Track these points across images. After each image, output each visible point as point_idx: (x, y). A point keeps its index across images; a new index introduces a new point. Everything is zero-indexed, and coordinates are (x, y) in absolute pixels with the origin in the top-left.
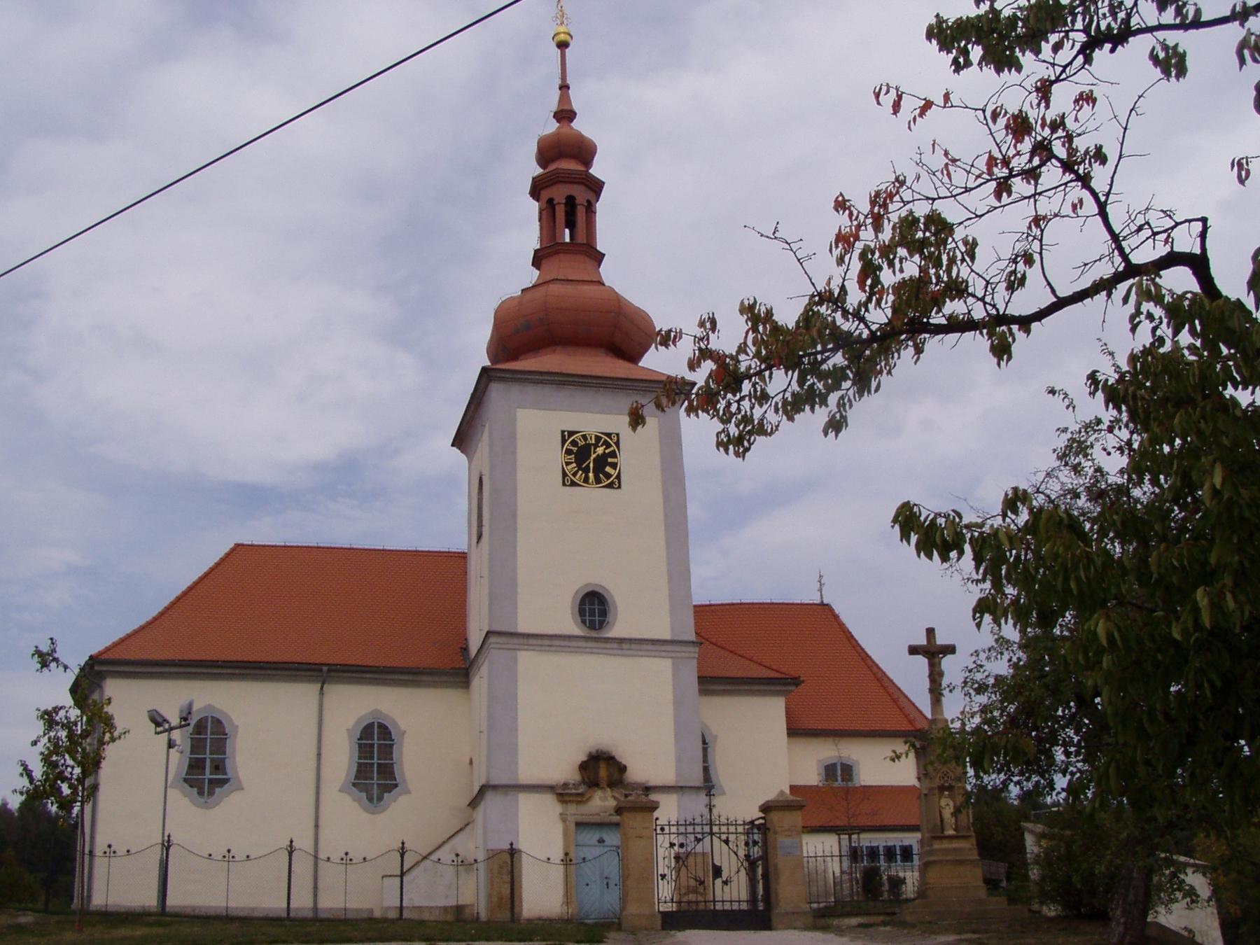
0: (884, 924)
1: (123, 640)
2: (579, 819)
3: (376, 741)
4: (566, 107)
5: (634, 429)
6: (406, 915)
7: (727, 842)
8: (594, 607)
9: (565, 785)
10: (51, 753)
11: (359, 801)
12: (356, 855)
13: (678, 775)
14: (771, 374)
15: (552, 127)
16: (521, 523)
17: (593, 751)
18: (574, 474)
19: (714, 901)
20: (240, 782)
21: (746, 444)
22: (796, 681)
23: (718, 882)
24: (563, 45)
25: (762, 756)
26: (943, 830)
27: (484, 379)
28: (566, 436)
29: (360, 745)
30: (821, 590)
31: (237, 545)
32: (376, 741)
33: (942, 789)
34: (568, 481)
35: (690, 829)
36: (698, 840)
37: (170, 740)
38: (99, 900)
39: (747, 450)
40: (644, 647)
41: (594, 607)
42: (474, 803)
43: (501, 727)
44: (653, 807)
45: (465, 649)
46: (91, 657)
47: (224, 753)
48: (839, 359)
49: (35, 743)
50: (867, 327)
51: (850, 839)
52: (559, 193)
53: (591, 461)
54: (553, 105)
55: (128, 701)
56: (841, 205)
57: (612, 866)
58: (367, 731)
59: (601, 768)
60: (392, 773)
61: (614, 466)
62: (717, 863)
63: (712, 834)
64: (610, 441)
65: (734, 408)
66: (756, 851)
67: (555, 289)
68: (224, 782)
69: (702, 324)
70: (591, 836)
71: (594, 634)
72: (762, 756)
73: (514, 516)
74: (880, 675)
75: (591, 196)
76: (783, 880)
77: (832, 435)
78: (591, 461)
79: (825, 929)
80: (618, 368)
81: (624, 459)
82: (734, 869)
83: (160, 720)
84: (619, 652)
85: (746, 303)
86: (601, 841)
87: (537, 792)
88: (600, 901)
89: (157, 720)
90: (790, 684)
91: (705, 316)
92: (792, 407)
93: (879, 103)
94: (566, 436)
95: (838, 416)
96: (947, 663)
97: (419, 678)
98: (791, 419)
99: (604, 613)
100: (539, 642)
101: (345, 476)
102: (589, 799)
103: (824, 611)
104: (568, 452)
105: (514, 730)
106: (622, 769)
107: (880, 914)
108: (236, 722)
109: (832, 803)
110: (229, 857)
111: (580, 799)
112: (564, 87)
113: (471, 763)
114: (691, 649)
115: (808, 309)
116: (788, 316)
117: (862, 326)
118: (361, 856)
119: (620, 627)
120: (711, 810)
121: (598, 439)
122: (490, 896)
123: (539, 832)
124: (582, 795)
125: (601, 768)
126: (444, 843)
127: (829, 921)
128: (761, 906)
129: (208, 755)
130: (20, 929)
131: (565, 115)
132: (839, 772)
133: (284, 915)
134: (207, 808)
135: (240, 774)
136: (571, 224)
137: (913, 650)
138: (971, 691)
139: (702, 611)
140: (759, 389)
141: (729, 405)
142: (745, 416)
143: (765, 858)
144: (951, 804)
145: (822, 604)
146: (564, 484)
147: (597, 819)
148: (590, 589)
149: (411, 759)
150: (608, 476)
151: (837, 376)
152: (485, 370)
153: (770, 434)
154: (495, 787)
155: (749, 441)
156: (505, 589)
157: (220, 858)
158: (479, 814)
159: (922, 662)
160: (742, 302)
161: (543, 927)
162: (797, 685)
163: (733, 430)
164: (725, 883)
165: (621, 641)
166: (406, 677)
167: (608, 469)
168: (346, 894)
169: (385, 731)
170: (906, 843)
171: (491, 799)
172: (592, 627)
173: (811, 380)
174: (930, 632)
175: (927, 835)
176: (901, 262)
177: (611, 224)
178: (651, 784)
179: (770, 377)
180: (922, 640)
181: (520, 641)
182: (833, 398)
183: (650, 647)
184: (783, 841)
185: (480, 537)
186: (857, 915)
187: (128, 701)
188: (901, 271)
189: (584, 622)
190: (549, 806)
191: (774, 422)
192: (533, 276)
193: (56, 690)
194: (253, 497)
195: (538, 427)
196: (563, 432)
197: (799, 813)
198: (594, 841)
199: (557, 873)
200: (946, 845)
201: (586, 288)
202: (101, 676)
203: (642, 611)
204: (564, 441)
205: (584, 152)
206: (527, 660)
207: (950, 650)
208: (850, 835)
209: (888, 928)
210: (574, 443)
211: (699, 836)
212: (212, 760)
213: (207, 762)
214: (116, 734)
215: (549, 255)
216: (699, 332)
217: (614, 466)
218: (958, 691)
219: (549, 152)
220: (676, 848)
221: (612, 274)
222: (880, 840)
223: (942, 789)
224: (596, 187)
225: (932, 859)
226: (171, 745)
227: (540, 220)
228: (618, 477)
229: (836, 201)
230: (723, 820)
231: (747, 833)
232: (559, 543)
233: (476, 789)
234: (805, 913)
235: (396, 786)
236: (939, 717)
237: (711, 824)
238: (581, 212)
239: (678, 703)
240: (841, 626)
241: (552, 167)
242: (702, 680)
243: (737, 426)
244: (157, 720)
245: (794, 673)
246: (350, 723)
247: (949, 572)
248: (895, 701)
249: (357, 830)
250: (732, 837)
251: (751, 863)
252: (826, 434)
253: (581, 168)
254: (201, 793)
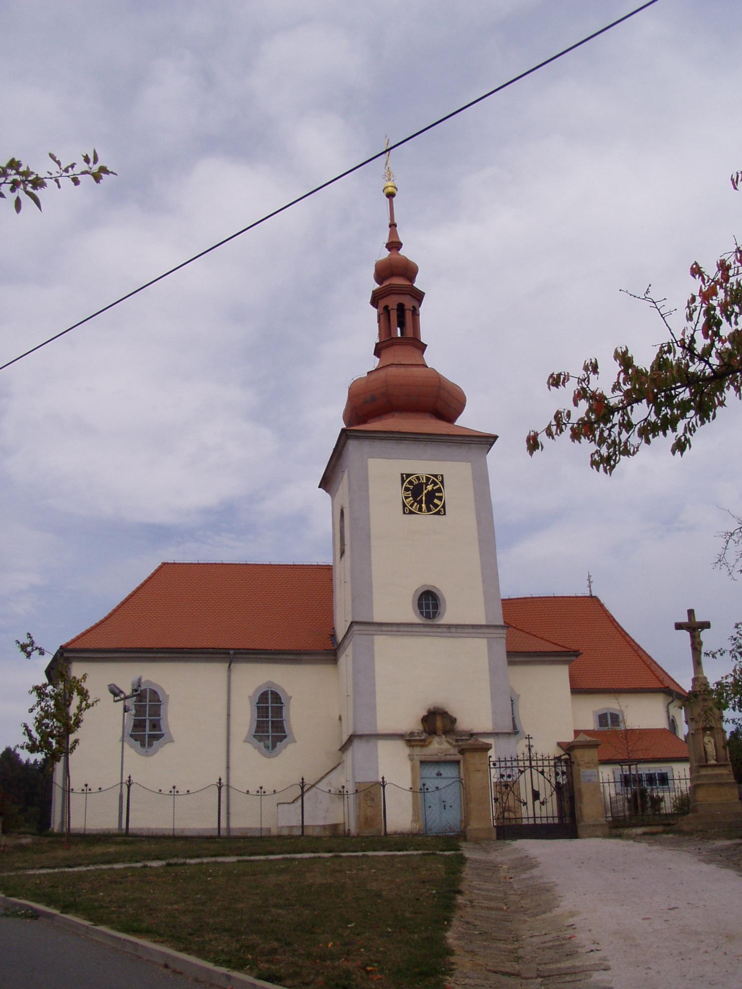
0: (667, 832)
1: (83, 634)
2: (423, 758)
3: (270, 704)
4: (395, 240)
5: (531, 454)
6: (307, 832)
7: (542, 773)
8: (429, 602)
9: (412, 734)
10: (43, 718)
11: (259, 749)
12: (269, 789)
13: (494, 724)
14: (632, 408)
15: (385, 254)
16: (374, 542)
17: (431, 707)
18: (412, 506)
19: (535, 817)
20: (171, 737)
21: (612, 463)
22: (576, 653)
23: (537, 803)
24: (391, 196)
25: (553, 710)
26: (707, 760)
27: (343, 437)
28: (404, 477)
29: (258, 707)
30: (590, 587)
31: (164, 564)
32: (270, 704)
33: (705, 729)
34: (407, 511)
35: (515, 764)
36: (521, 772)
37: (125, 706)
38: (77, 823)
39: (614, 466)
40: (467, 630)
41: (429, 602)
42: (344, 748)
43: (363, 691)
44: (486, 748)
45: (333, 636)
46: (61, 647)
47: (159, 715)
48: (685, 394)
49: (31, 710)
50: (711, 367)
51: (630, 768)
52: (392, 302)
53: (423, 496)
54: (385, 238)
55: (96, 677)
56: (696, 271)
57: (452, 794)
58: (263, 697)
59: (437, 721)
60: (282, 727)
61: (440, 498)
62: (536, 788)
63: (531, 767)
64: (437, 480)
65: (606, 434)
66: (562, 780)
67: (393, 371)
68: (157, 737)
69: (586, 368)
70: (431, 771)
71: (430, 622)
72: (553, 710)
73: (369, 536)
74: (636, 648)
75: (416, 304)
76: (586, 800)
77: (678, 453)
78: (423, 496)
79: (619, 836)
80: (440, 427)
81: (447, 494)
82: (548, 793)
83: (117, 692)
84: (449, 635)
85: (619, 351)
86: (439, 774)
87: (391, 739)
88: (445, 818)
89: (115, 692)
90: (572, 655)
91: (588, 361)
92: (648, 431)
93: (735, 188)
94: (404, 477)
95: (683, 438)
96: (704, 635)
97: (301, 657)
98: (648, 441)
99: (436, 606)
100: (390, 629)
101: (224, 517)
102: (430, 743)
103: (593, 601)
104: (407, 489)
105: (373, 694)
106: (453, 721)
107: (658, 825)
108: (167, 693)
109: (610, 740)
110: (261, 792)
111: (423, 744)
112: (393, 225)
113: (340, 719)
114: (501, 631)
115: (659, 357)
116: (644, 361)
117: (707, 366)
118: (264, 792)
119: (448, 616)
120: (530, 750)
121: (428, 479)
122: (358, 818)
123: (394, 767)
124: (424, 740)
125: (437, 721)
126: (322, 778)
127: (621, 831)
128: (567, 820)
129: (147, 717)
130: (22, 848)
131: (394, 245)
132: (608, 719)
133: (216, 833)
134: (148, 756)
135: (172, 730)
136: (401, 324)
137: (679, 626)
138: (737, 654)
139: (509, 605)
140: (626, 418)
141: (602, 432)
142: (614, 441)
143: (571, 784)
144: (712, 741)
145: (591, 597)
146: (404, 513)
147: (435, 758)
148: (426, 589)
149: (296, 717)
150: (436, 506)
151: (684, 407)
152: (343, 431)
153: (634, 453)
154: (361, 736)
155: (615, 461)
156: (363, 590)
157: (168, 793)
158: (348, 756)
159: (685, 635)
160: (616, 351)
161: (403, 841)
162: (577, 656)
163: (604, 451)
164: (542, 803)
165: (449, 626)
166: (291, 657)
167: (436, 501)
168: (246, 818)
169: (276, 697)
170: (664, 771)
171: (357, 744)
172: (428, 616)
173: (665, 411)
174: (691, 613)
175: (696, 764)
176: (736, 317)
177: (431, 321)
178: (475, 731)
179: (632, 410)
180: (685, 619)
181: (376, 628)
182: (681, 425)
183: (471, 630)
184: (585, 773)
185: (342, 553)
186: (641, 826)
187: (96, 677)
188: (736, 323)
189: (422, 613)
190: (400, 749)
191: (636, 444)
192: (375, 362)
193: (36, 671)
194: (160, 533)
195: (384, 471)
196: (402, 475)
197: (596, 750)
198: (434, 774)
199: (407, 798)
200: (710, 772)
201: (414, 369)
202: (69, 661)
203: (464, 605)
204: (403, 482)
205: (409, 271)
206: (382, 643)
207: (707, 625)
208: (630, 766)
209: (671, 836)
210: (410, 483)
211: (522, 769)
212: (151, 721)
213: (146, 722)
214: (90, 701)
215: (387, 347)
216: (582, 374)
217: (440, 498)
218: (727, 654)
219: (383, 272)
220: (505, 778)
221: (433, 359)
222: (644, 769)
223: (705, 729)
224: (419, 296)
225: (698, 782)
226: (126, 710)
227: (379, 322)
228: (444, 507)
229: (692, 268)
230: (539, 757)
231: (555, 766)
232: (403, 556)
233: (345, 738)
234: (602, 825)
235: (285, 737)
236: (700, 676)
237: (530, 760)
238: (408, 315)
239: (493, 670)
240: (606, 612)
241: (386, 283)
242: (509, 654)
243: (608, 449)
244: (115, 692)
245: (576, 648)
246: (251, 692)
247: (718, 565)
248: (648, 667)
249: (254, 769)
250: (546, 769)
251: (558, 788)
252: (674, 453)
253: (408, 283)
254: (143, 745)
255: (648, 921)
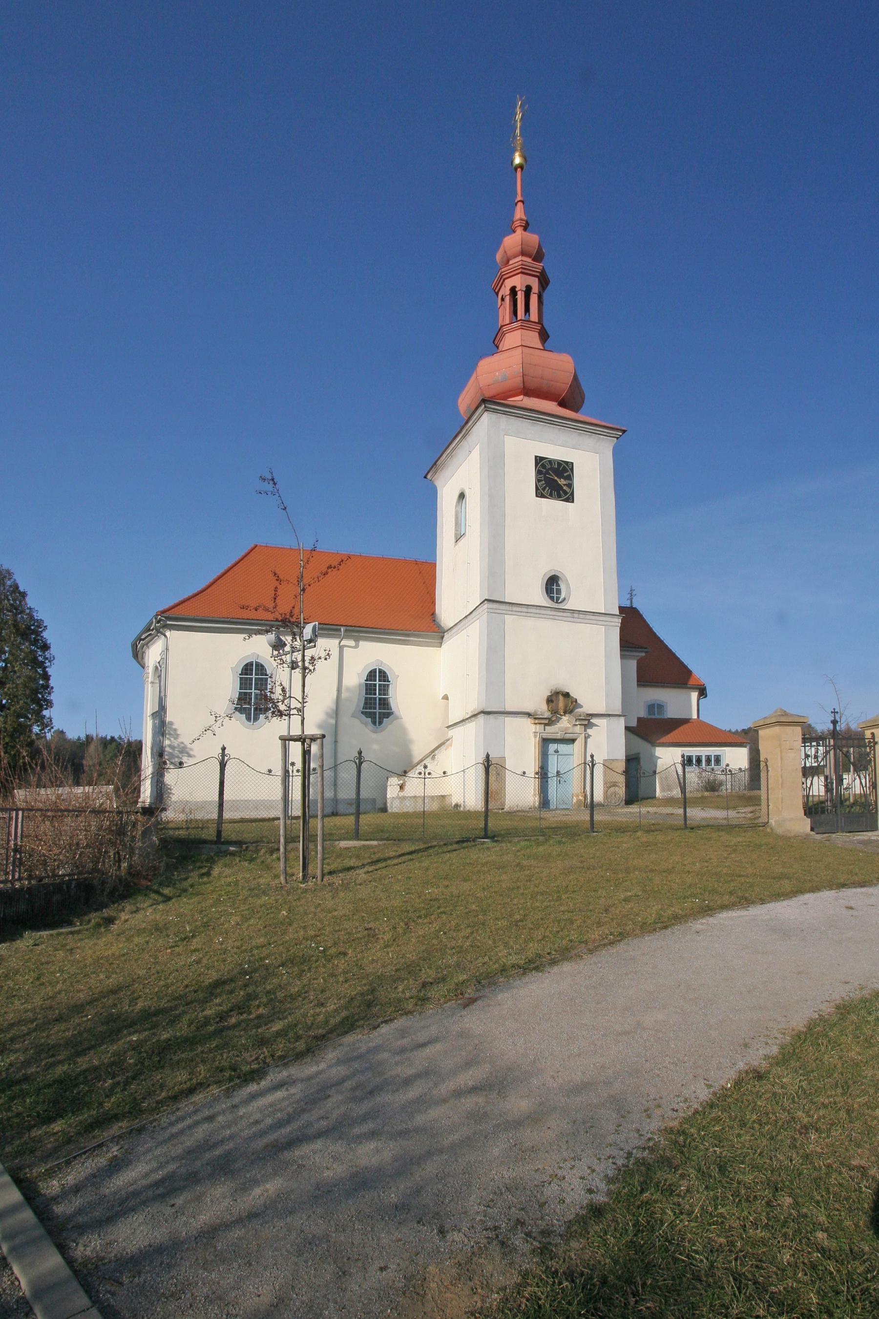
18: (544, 489)
24: (285, 509)
28: (539, 460)
111: (550, 722)
114: (616, 620)
169: (383, 676)
181: (507, 607)
255: (851, 912)
